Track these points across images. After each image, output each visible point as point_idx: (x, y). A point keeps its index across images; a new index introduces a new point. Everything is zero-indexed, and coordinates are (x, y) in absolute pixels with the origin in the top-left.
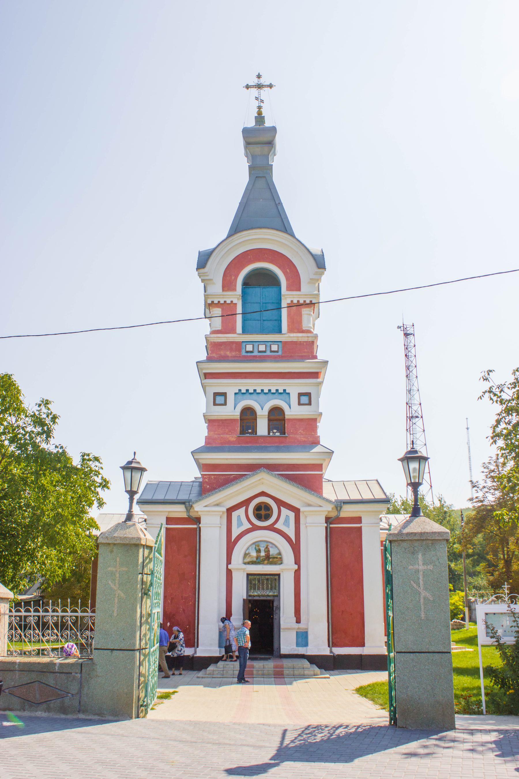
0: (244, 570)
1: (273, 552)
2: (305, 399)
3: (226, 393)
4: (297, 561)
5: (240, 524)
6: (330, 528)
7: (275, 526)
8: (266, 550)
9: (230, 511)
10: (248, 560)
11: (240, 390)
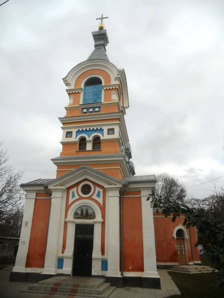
0: (73, 222)
1: (90, 212)
2: (111, 132)
3: (114, 129)
4: (103, 216)
5: (73, 196)
6: (123, 198)
7: (92, 197)
8: (87, 210)
9: (69, 189)
10: (77, 216)
11: (79, 130)
